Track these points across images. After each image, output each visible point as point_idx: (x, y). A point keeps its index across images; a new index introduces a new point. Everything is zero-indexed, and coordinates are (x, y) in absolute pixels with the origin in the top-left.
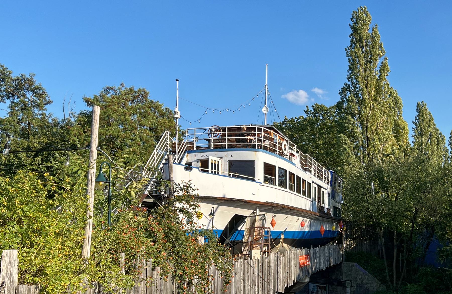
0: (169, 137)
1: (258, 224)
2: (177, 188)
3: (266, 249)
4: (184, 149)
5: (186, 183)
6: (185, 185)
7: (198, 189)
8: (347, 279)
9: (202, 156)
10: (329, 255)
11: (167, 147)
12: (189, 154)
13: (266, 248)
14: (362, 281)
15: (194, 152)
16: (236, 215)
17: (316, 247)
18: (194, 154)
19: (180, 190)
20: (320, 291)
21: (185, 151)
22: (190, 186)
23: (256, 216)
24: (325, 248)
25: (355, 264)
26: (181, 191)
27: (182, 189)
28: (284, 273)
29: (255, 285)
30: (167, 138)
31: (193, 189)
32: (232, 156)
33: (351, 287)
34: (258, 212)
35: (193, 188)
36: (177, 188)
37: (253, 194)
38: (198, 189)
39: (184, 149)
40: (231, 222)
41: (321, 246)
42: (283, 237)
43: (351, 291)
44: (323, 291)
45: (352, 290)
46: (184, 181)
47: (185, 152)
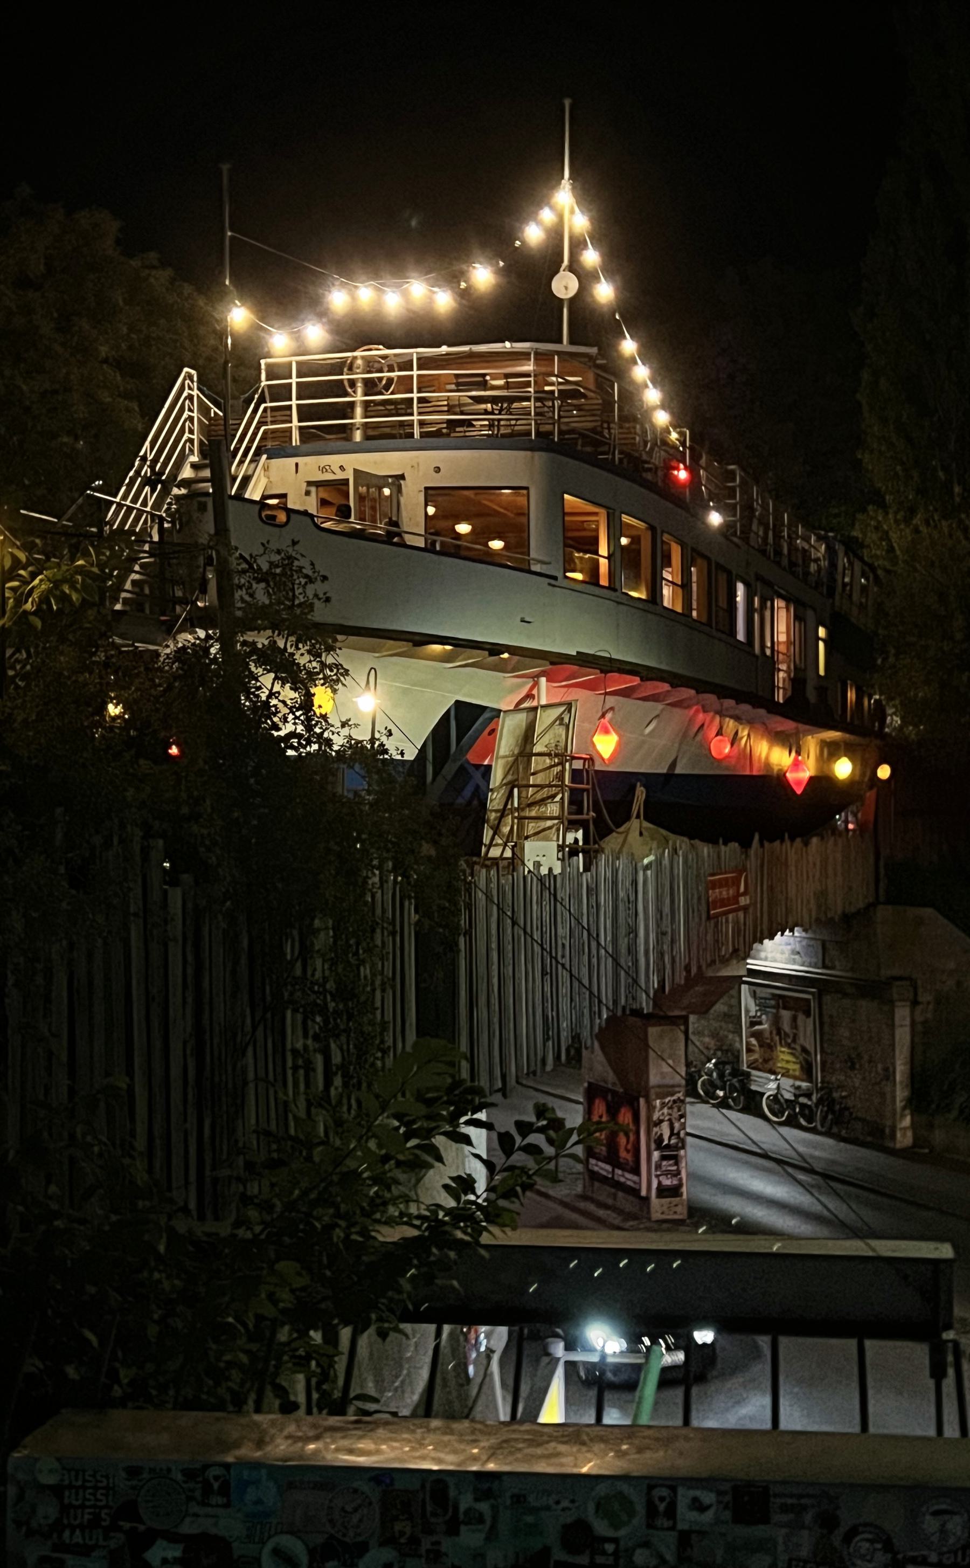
0: (195, 392)
1: (546, 739)
2: (244, 572)
3: (576, 840)
4: (252, 440)
5: (279, 552)
6: (276, 558)
7: (325, 578)
8: (896, 972)
9: (323, 469)
10: (452, 1432)
11: (191, 432)
12: (274, 462)
13: (580, 835)
14: (959, 984)
15: (295, 453)
16: (458, 703)
17: (771, 841)
18: (293, 460)
19: (259, 581)
20: (786, 1015)
21: (258, 448)
22: (296, 563)
23: (535, 709)
24: (806, 844)
25: (928, 911)
26: (263, 585)
27: (263, 578)
28: (652, 937)
29: (544, 973)
30: (190, 397)
31: (306, 576)
32: (437, 470)
33: (915, 1003)
34: (545, 692)
35: (308, 571)
36: (244, 572)
37: (523, 621)
38: (325, 578)
39: (252, 440)
40: (440, 732)
41: (792, 839)
42: (640, 793)
43: (913, 1023)
44: (801, 1017)
45: (919, 1018)
46: (274, 546)
47: (258, 453)
